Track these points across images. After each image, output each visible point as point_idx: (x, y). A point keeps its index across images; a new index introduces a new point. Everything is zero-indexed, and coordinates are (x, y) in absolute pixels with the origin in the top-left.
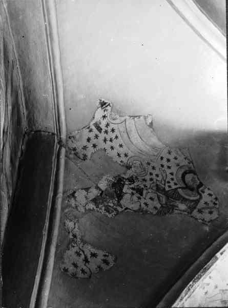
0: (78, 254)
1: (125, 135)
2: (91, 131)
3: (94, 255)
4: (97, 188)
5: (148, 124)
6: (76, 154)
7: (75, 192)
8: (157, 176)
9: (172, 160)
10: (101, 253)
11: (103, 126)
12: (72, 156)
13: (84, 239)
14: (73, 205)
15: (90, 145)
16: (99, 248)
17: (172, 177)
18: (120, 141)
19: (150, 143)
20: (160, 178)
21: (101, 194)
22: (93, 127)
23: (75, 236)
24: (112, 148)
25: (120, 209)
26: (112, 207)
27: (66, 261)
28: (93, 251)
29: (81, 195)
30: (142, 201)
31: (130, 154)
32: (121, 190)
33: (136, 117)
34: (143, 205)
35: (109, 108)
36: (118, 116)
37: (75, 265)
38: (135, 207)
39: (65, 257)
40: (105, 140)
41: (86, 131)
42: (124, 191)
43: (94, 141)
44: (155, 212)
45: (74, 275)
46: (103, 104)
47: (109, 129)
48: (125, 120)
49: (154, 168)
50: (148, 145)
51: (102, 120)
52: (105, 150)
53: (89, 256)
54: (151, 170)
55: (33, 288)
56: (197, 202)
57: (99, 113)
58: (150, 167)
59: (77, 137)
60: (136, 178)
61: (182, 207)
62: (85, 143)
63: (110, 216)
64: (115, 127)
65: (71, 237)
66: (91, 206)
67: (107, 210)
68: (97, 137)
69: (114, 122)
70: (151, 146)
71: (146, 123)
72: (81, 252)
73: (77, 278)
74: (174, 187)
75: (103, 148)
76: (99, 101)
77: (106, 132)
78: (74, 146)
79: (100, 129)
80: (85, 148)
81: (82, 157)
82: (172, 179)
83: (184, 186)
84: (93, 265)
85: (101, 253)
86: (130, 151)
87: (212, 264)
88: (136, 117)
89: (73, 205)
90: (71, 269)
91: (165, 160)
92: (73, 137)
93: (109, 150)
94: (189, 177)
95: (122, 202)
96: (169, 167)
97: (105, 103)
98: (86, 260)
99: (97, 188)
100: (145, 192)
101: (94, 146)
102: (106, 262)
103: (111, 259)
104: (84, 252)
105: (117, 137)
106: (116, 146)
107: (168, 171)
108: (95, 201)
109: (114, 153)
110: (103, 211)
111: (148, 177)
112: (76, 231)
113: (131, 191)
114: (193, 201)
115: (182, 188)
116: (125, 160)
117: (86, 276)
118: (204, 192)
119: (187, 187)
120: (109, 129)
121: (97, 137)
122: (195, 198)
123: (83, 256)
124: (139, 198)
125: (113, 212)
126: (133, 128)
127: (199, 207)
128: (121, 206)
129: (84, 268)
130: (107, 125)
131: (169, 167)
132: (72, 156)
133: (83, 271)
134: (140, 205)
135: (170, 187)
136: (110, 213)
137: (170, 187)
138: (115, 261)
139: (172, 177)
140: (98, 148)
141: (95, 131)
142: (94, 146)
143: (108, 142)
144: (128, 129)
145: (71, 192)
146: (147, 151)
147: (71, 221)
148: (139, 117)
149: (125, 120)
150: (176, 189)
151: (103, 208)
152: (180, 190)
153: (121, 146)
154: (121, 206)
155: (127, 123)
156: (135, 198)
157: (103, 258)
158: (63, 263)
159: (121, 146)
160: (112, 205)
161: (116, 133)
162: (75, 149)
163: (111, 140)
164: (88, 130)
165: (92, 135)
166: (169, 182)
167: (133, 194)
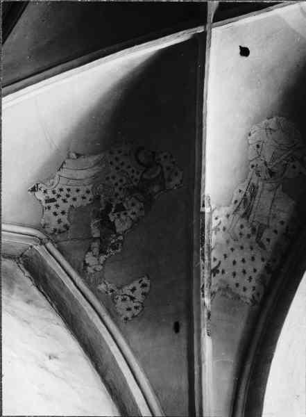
0: (124, 300)
1: (71, 181)
2: (49, 208)
3: (133, 290)
4: (95, 239)
5: (75, 157)
6: (60, 232)
7: (85, 261)
8: (121, 181)
9: (119, 156)
10: (136, 284)
11: (51, 196)
12: (58, 237)
13: (119, 286)
14: (92, 271)
15: (60, 216)
16: (132, 281)
17: (131, 169)
18: (73, 189)
19: (93, 164)
20: (125, 181)
21: (101, 241)
22: (48, 204)
23: (112, 291)
24: (74, 199)
25: (121, 238)
26: (115, 242)
27: (121, 312)
28: (131, 287)
29: (90, 259)
30: (129, 213)
31: (90, 187)
32: (109, 221)
33: (62, 165)
34: (132, 216)
35: (39, 186)
36: (52, 181)
37: (129, 309)
38: (128, 225)
39: (119, 311)
40: (65, 201)
41: (47, 212)
42: (112, 220)
43: (59, 211)
44: (143, 213)
45: (133, 317)
46: (34, 190)
47: (58, 192)
48: (60, 176)
49: (114, 178)
50: (93, 166)
51: (46, 195)
52: (72, 206)
53: (131, 294)
54: (114, 182)
55: (118, 368)
56: (162, 173)
57: (40, 195)
58: (111, 180)
59: (47, 222)
60: (111, 200)
61: (156, 189)
62: (56, 218)
63: (119, 250)
64: (59, 186)
65: (110, 294)
66: (103, 258)
67: (115, 248)
68: (57, 206)
69: (54, 186)
70: (95, 165)
71: (74, 159)
72: (125, 297)
73: (137, 316)
74: (138, 177)
75: (69, 206)
76: (29, 192)
77: (59, 196)
78: (52, 228)
79: (53, 200)
80: (59, 221)
81: (64, 229)
82: (133, 171)
83: (144, 168)
84: (139, 298)
85: (136, 284)
86: (87, 187)
87: (244, 18)
88: (62, 165)
89: (92, 271)
90: (129, 314)
91: (114, 162)
92: (45, 225)
93: (75, 204)
94: (142, 158)
95: (117, 231)
96: (122, 164)
97: (34, 187)
98: (132, 298)
99: (95, 239)
100: (125, 205)
101: (63, 213)
102: (144, 286)
103: (145, 281)
104: (125, 295)
105: (69, 190)
106: (75, 194)
107: (124, 168)
108: (102, 252)
109: (79, 200)
110: (113, 252)
111: (117, 190)
112: (110, 286)
113: (116, 214)
114: (158, 177)
115: (145, 172)
116: (90, 196)
117: (140, 309)
118: (160, 159)
119: (147, 167)
120: (58, 192)
121: (57, 206)
122: (158, 172)
123: (128, 298)
124: (125, 214)
125: (118, 245)
126: (70, 172)
127: (166, 176)
128: (118, 235)
129: (135, 304)
130: (54, 192)
131: (122, 164)
132: (58, 237)
133: (136, 308)
134: (131, 219)
135: (136, 180)
136: (118, 249)
137: (136, 180)
138: (149, 278)
139: (131, 169)
140: (67, 211)
141: (52, 205)
142: (63, 213)
143: (68, 200)
144: (69, 176)
145: (82, 264)
146: (97, 171)
147: (100, 284)
148: (64, 162)
149: (60, 176)
150: (141, 177)
151: (111, 250)
152: (145, 176)
153: (78, 191)
154: (119, 235)
155: (63, 175)
156: (123, 217)
157: (141, 285)
158: (121, 316)
159: (78, 191)
160: (113, 241)
161: (65, 188)
162: (55, 230)
163: (68, 196)
164: (47, 210)
165: (53, 209)
166: (132, 177)
167: (119, 215)
